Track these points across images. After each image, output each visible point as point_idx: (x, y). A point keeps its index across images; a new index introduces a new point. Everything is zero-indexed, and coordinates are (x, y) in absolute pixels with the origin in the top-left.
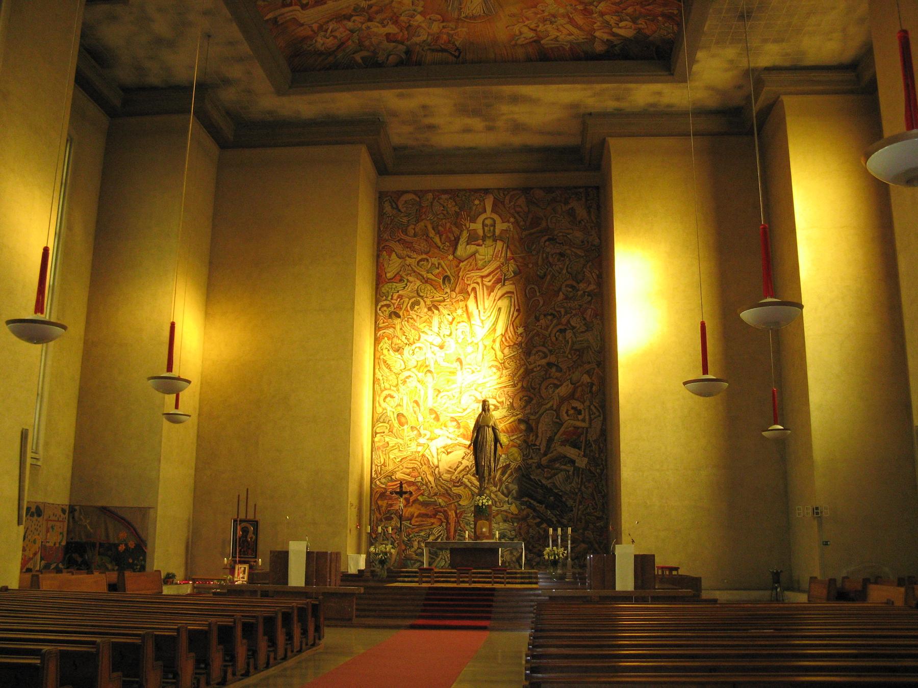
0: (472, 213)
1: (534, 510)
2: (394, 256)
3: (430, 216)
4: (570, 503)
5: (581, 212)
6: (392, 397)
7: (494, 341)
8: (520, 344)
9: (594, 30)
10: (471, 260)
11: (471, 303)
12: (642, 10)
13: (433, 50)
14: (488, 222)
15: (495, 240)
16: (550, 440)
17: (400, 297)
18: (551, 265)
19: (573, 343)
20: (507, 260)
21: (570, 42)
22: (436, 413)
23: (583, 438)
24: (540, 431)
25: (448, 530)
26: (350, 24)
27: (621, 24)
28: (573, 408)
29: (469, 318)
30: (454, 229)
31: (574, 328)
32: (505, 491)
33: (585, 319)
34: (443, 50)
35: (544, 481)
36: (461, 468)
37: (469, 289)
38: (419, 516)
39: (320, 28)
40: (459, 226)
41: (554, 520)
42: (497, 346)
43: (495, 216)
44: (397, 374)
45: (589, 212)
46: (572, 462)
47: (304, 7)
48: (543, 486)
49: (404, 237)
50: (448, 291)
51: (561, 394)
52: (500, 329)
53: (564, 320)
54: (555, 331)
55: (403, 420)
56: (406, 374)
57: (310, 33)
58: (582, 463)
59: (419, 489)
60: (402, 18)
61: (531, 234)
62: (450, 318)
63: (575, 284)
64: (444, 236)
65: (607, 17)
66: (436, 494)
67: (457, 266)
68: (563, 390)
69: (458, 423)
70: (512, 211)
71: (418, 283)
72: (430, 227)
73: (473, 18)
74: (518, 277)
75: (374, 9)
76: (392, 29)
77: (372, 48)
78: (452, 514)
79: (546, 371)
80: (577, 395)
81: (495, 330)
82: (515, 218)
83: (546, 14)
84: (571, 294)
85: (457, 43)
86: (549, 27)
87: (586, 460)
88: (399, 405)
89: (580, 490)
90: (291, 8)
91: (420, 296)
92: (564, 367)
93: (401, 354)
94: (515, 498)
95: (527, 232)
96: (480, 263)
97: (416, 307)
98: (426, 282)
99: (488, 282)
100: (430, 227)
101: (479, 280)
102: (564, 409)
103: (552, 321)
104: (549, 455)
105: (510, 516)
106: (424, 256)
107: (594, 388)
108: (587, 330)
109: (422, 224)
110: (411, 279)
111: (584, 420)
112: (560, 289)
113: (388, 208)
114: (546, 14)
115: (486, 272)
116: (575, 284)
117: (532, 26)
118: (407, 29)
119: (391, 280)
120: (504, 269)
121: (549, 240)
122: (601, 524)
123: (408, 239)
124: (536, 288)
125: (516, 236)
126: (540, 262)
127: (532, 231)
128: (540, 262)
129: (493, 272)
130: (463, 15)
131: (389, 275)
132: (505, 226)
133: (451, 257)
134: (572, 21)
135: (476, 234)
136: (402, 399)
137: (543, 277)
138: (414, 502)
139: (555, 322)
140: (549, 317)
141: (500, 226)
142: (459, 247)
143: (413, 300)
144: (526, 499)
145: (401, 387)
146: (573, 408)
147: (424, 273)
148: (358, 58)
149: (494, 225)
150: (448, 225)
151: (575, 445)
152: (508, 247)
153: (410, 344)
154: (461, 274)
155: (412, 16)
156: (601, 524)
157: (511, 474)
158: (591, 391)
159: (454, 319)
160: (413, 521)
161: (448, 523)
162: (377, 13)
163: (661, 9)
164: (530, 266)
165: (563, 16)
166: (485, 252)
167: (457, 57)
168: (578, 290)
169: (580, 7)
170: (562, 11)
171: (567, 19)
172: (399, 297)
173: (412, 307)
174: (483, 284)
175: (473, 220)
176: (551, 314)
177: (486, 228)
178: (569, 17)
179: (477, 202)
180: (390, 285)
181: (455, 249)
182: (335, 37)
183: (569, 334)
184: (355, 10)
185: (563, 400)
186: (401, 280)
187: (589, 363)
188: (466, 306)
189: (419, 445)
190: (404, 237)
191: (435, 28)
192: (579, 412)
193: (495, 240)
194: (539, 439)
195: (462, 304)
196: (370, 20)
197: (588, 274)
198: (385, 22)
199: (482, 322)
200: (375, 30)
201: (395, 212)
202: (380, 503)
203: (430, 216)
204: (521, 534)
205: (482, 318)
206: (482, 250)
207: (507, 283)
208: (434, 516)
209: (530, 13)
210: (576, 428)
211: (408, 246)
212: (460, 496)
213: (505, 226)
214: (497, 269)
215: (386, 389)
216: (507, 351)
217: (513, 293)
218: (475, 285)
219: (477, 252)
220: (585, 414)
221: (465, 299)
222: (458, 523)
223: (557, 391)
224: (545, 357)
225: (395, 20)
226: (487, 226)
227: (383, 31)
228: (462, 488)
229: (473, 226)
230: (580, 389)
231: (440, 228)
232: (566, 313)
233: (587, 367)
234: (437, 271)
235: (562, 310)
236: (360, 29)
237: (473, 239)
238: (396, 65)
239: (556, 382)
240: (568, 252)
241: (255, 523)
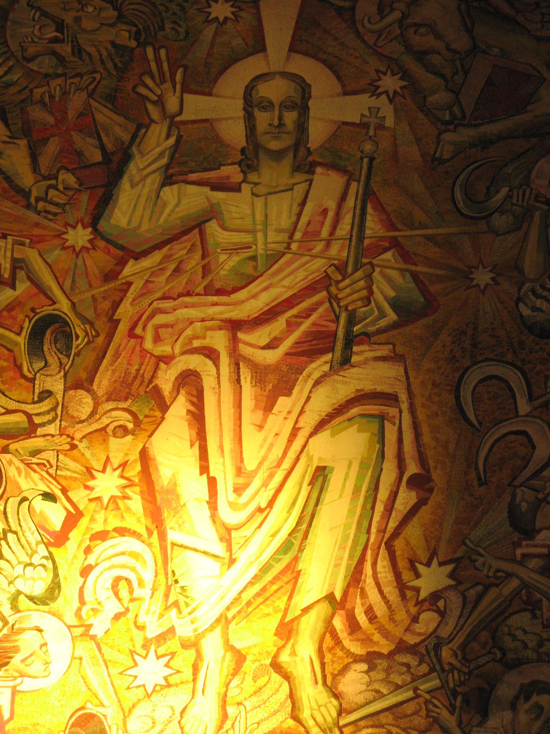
0: (200, 52)
7: (286, 630)
8: (429, 650)
10: (179, 250)
11: (172, 450)
14: (274, 91)
15: (305, 166)
20: (364, 253)
29: (155, 515)
30: (104, 116)
42: (303, 654)
43: (304, 67)
50: (57, 385)
52: (322, 570)
61: (485, 143)
62: (55, 515)
64: (52, 147)
67: (110, 276)
69: (524, 630)
74: (417, 328)
81: (292, 574)
82: (405, 75)
95: (466, 134)
96: (227, 265)
99: (262, 348)
101: (219, 341)
115: (250, 303)
120: (350, 291)
124: (515, 378)
125: (412, 152)
127: (492, 129)
129: (289, 303)
132: (355, 108)
133: (80, 236)
141: (330, 109)
149: (301, 102)
150: (77, 101)
152: (368, 195)
154: (126, 311)
159: (72, 519)
164: (483, 277)
166: (253, 215)
174: (237, 360)
175: (203, 82)
177: (263, 119)
181: (104, 201)
188: (145, 456)
193: (305, 166)
195: (121, 448)
199: (226, 534)
205: (226, 514)
206: (238, 207)
207: (361, 353)
213: (355, 108)
214: (310, 289)
216: (354, 683)
217: (391, 399)
218: (196, 362)
219: (212, 213)
221: (144, 425)
226: (267, 105)
229: (196, 106)
231: (37, 114)
237: (194, 157)
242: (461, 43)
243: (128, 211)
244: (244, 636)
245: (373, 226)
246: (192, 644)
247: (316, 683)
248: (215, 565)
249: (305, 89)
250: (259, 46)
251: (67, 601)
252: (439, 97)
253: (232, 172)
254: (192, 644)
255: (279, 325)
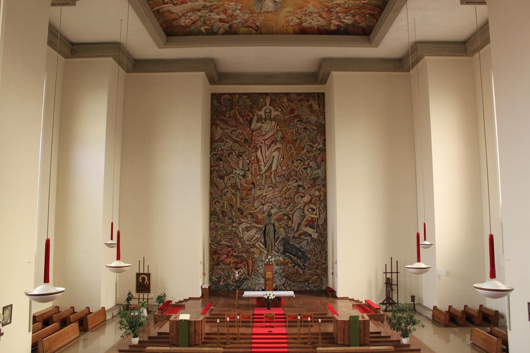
0: (259, 106)
1: (291, 259)
2: (219, 128)
3: (238, 107)
4: (309, 256)
5: (315, 107)
6: (219, 202)
9: (332, 20)
10: (258, 131)
12: (359, 12)
13: (244, 27)
14: (268, 111)
15: (271, 121)
16: (299, 224)
17: (222, 150)
18: (300, 134)
19: (311, 175)
21: (318, 25)
22: (241, 210)
23: (315, 223)
24: (294, 220)
25: (248, 270)
26: (199, 14)
27: (346, 18)
28: (311, 208)
30: (250, 114)
31: (311, 167)
32: (277, 250)
33: (317, 162)
34: (249, 27)
35: (296, 245)
36: (254, 238)
37: (258, 146)
38: (233, 263)
39: (183, 15)
40: (253, 113)
41: (301, 264)
44: (221, 190)
45: (319, 107)
46: (310, 235)
47: (175, 5)
48: (295, 248)
49: (223, 118)
51: (305, 201)
53: (306, 163)
54: (302, 168)
55: (225, 214)
56: (227, 190)
57: (177, 17)
58: (315, 236)
59: (233, 249)
60: (229, 11)
61: (290, 118)
62: (248, 161)
63: (312, 144)
64: (245, 118)
65: (340, 14)
66: (242, 252)
68: (306, 199)
70: (280, 105)
71: (232, 143)
72: (237, 113)
73: (268, 12)
75: (214, 7)
76: (223, 16)
77: (211, 25)
78: (250, 262)
79: (297, 189)
80: (313, 201)
83: (307, 11)
84: (310, 150)
85: (257, 24)
86: (308, 18)
87: (317, 234)
88: (222, 206)
89: (314, 249)
90: (167, 5)
91: (232, 150)
92: (306, 188)
93: (223, 180)
94: (282, 254)
96: (264, 133)
97: (231, 155)
98: (236, 142)
100: (237, 113)
101: (263, 142)
102: (306, 208)
103: (300, 163)
104: (299, 232)
105: (279, 262)
106: (234, 129)
107: (321, 198)
108: (318, 168)
109: (233, 111)
110: (227, 140)
111: (316, 214)
112: (304, 147)
113: (215, 102)
114: (307, 11)
116: (312, 144)
117: (299, 17)
118: (231, 16)
119: (217, 141)
121: (298, 121)
122: (325, 266)
123: (226, 119)
124: (292, 146)
126: (294, 132)
127: (290, 116)
128: (294, 132)
130: (262, 11)
131: (216, 138)
133: (248, 129)
134: (320, 16)
135: (262, 117)
136: (224, 203)
137: (296, 140)
138: (231, 256)
139: (302, 164)
140: (299, 161)
141: (274, 113)
142: (253, 124)
143: (228, 152)
144: (287, 254)
145: (224, 198)
146: (311, 208)
147: (234, 138)
148: (203, 29)
149: (270, 112)
150: (247, 112)
151: (311, 227)
152: (278, 124)
153: (228, 175)
155: (235, 11)
156: (325, 266)
157: (280, 242)
158: (320, 199)
160: (231, 265)
161: (248, 266)
162: (215, 9)
163: (369, 12)
164: (289, 134)
165: (316, 13)
167: (257, 30)
168: (313, 147)
169: (326, 9)
170: (316, 10)
171: (318, 15)
172: (221, 150)
173: (229, 155)
175: (260, 110)
176: (300, 160)
177: (267, 114)
178: (319, 14)
179: (262, 100)
180: (217, 144)
181: (250, 125)
182: (191, 19)
183: (309, 170)
184: (203, 7)
185: (306, 204)
186: (223, 141)
187: (319, 185)
188: (257, 155)
189: (233, 227)
190: (223, 118)
191: (246, 16)
192: (314, 210)
193: (271, 121)
194: (294, 224)
196: (211, 12)
197: (318, 139)
198: (219, 13)
200: (213, 16)
201: (219, 104)
202: (213, 256)
203: (238, 107)
204: (285, 272)
206: (264, 125)
208: (241, 263)
209: (299, 11)
210: (313, 218)
211: (226, 123)
212: (254, 253)
214: (272, 136)
215: (215, 198)
217: (280, 148)
219: (262, 126)
220: (317, 211)
222: (253, 266)
223: (303, 199)
224: (297, 182)
225: (225, 12)
227: (217, 17)
228: (255, 248)
229: (260, 113)
230: (314, 198)
231: (243, 114)
232: (307, 159)
233: (318, 187)
234: (241, 136)
235: (306, 158)
236: (205, 16)
237: (259, 120)
238: (223, 34)
239: (302, 195)
240: (308, 127)
241: (148, 275)
242: (287, 105)
243: (253, 127)
244: (267, 174)
245: (278, 128)
246: (262, 175)
247: (29, 331)
248: (1, 320)
249: (271, 111)
250: (266, 105)
251: (250, 171)
252: (285, 112)
253: (263, 121)
254: (262, 175)
255: (269, 140)
